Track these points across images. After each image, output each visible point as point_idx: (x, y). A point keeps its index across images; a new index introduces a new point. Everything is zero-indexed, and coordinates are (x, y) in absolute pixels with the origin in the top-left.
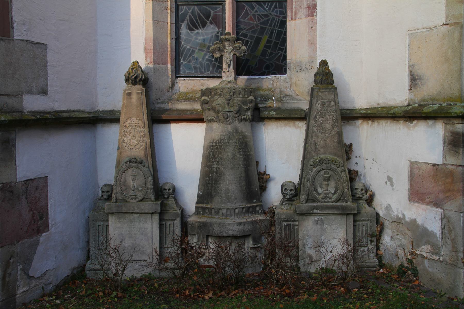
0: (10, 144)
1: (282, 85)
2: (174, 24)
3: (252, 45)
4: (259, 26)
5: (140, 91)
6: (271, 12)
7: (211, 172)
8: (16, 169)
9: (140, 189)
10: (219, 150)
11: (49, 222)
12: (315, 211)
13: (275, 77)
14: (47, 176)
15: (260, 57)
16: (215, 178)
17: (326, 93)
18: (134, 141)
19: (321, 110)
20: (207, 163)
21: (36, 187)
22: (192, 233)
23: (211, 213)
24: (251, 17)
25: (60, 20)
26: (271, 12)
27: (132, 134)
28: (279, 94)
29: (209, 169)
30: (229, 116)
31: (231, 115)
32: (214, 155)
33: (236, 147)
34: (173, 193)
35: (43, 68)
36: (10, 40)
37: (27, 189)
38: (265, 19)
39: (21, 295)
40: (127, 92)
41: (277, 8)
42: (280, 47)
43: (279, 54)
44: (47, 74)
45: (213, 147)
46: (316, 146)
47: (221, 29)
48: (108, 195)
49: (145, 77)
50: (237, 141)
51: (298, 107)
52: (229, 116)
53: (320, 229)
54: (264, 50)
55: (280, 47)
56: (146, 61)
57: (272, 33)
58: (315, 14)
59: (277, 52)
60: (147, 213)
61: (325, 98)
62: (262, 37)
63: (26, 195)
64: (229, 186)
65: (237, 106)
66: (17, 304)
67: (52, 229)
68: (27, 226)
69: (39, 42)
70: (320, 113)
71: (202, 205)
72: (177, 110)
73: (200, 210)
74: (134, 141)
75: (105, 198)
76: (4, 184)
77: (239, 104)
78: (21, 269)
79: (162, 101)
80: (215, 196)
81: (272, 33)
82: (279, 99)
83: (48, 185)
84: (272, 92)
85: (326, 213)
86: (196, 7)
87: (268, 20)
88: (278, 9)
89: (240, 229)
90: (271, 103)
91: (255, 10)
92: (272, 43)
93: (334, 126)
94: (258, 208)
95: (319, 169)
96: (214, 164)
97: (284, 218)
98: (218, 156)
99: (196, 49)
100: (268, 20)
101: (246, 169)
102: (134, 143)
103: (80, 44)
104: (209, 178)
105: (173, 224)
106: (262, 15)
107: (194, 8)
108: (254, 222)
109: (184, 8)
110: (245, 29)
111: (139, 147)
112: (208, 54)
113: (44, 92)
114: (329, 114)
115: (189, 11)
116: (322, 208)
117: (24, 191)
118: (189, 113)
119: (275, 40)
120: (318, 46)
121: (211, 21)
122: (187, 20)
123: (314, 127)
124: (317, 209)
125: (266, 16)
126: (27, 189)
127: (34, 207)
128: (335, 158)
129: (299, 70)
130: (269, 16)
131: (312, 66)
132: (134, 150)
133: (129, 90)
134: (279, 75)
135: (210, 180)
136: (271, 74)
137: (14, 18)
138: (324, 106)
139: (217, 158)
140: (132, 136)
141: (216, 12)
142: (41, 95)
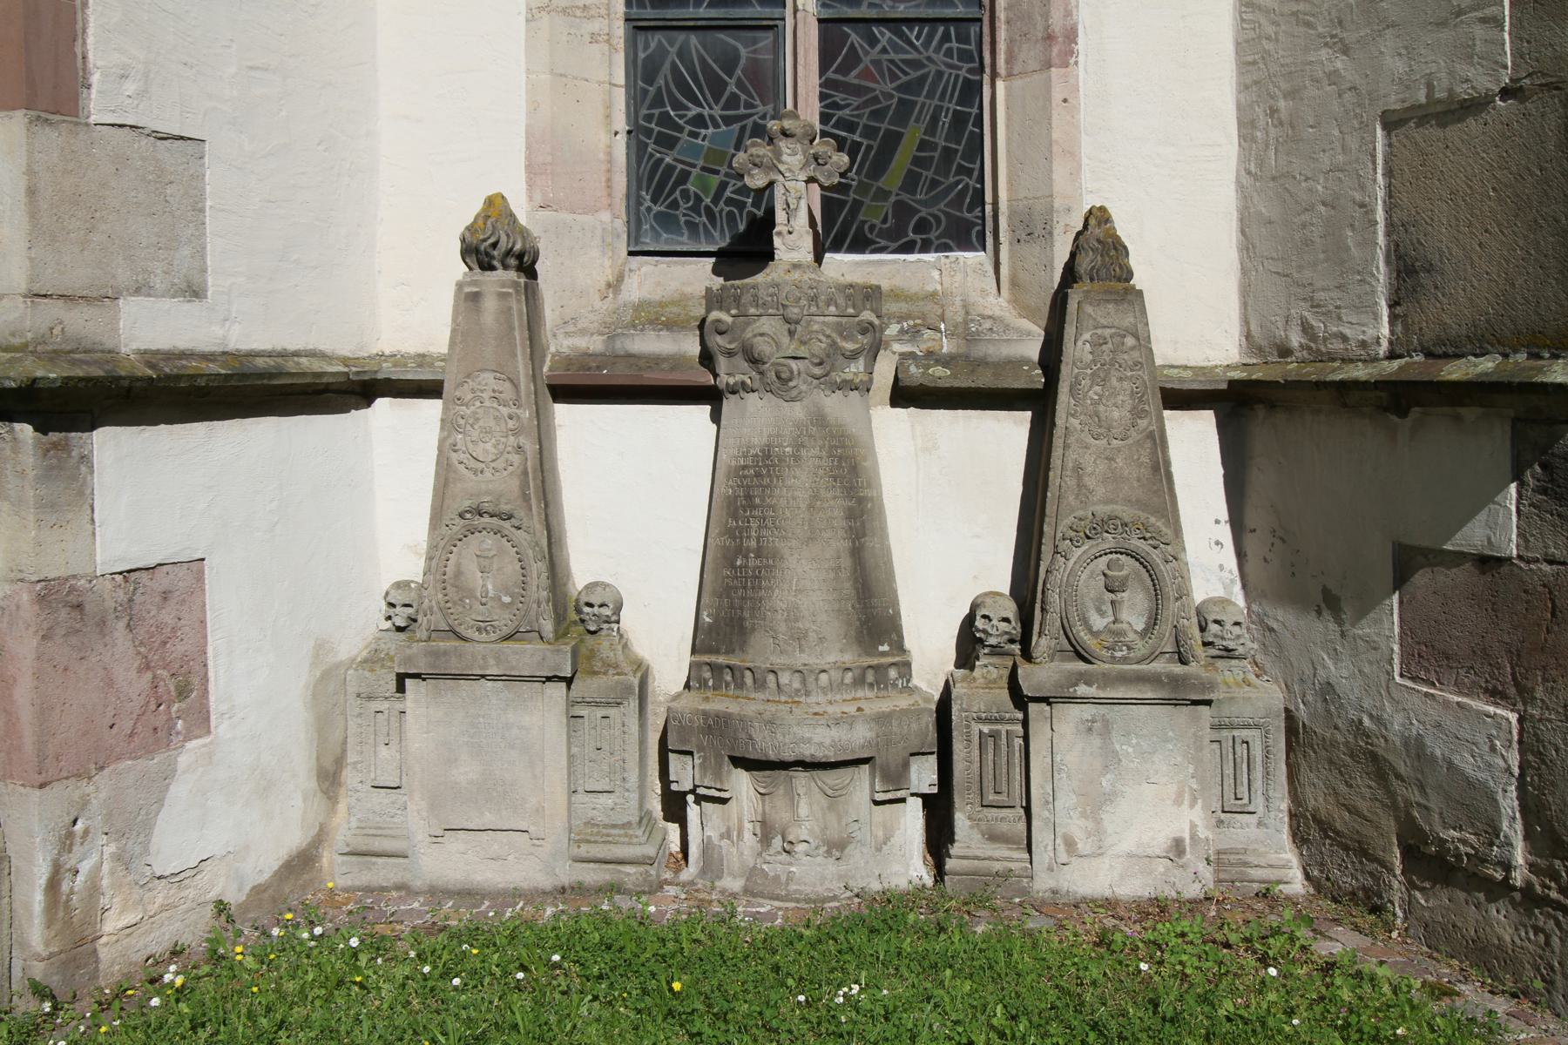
0: (74, 454)
3: (871, 157)
5: (509, 287)
6: (931, 53)
7: (741, 549)
8: (94, 534)
9: (507, 599)
10: (766, 481)
12: (1082, 690)
13: (947, 257)
15: (897, 195)
16: (754, 571)
18: (489, 446)
19: (1094, 362)
21: (164, 593)
23: (740, 685)
25: (251, 68)
26: (931, 53)
27: (481, 423)
31: (802, 369)
32: (749, 497)
35: (189, 214)
36: (77, 124)
37: (131, 600)
38: (914, 74)
39: (115, 938)
40: (468, 289)
41: (951, 42)
42: (963, 163)
43: (960, 187)
44: (205, 234)
46: (1079, 478)
48: (406, 616)
51: (1022, 357)
52: (796, 373)
53: (1100, 748)
54: (910, 171)
55: (963, 163)
56: (531, 199)
57: (935, 119)
58: (1072, 61)
59: (952, 180)
60: (531, 679)
61: (1105, 323)
62: (902, 130)
63: (128, 618)
64: (800, 596)
65: (820, 341)
66: (101, 967)
67: (221, 727)
68: (135, 716)
69: (176, 133)
70: (1089, 371)
71: (713, 658)
72: (630, 356)
73: (707, 675)
75: (397, 624)
76: (49, 581)
77: (828, 337)
78: (112, 855)
79: (580, 326)
80: (753, 629)
81: (935, 119)
82: (960, 330)
83: (207, 587)
84: (936, 307)
85: (1120, 695)
87: (923, 78)
88: (955, 45)
90: (934, 340)
91: (879, 47)
92: (935, 149)
93: (1137, 413)
94: (893, 673)
95: (1094, 551)
98: (763, 500)
100: (923, 78)
101: (853, 542)
102: (487, 452)
103: (319, 144)
104: (736, 572)
106: (902, 61)
109: (656, 40)
110: (848, 105)
112: (733, 182)
113: (194, 291)
114: (1120, 374)
115: (670, 49)
116: (1107, 680)
117: (121, 605)
119: (946, 140)
120: (1085, 161)
121: (739, 79)
122: (665, 76)
123: (1073, 415)
124: (1089, 684)
126: (131, 600)
127: (156, 657)
130: (924, 66)
132: (488, 474)
134: (962, 253)
135: (737, 577)
137: (91, 56)
139: (758, 506)
140: (482, 432)
141: (755, 52)
142: (181, 299)
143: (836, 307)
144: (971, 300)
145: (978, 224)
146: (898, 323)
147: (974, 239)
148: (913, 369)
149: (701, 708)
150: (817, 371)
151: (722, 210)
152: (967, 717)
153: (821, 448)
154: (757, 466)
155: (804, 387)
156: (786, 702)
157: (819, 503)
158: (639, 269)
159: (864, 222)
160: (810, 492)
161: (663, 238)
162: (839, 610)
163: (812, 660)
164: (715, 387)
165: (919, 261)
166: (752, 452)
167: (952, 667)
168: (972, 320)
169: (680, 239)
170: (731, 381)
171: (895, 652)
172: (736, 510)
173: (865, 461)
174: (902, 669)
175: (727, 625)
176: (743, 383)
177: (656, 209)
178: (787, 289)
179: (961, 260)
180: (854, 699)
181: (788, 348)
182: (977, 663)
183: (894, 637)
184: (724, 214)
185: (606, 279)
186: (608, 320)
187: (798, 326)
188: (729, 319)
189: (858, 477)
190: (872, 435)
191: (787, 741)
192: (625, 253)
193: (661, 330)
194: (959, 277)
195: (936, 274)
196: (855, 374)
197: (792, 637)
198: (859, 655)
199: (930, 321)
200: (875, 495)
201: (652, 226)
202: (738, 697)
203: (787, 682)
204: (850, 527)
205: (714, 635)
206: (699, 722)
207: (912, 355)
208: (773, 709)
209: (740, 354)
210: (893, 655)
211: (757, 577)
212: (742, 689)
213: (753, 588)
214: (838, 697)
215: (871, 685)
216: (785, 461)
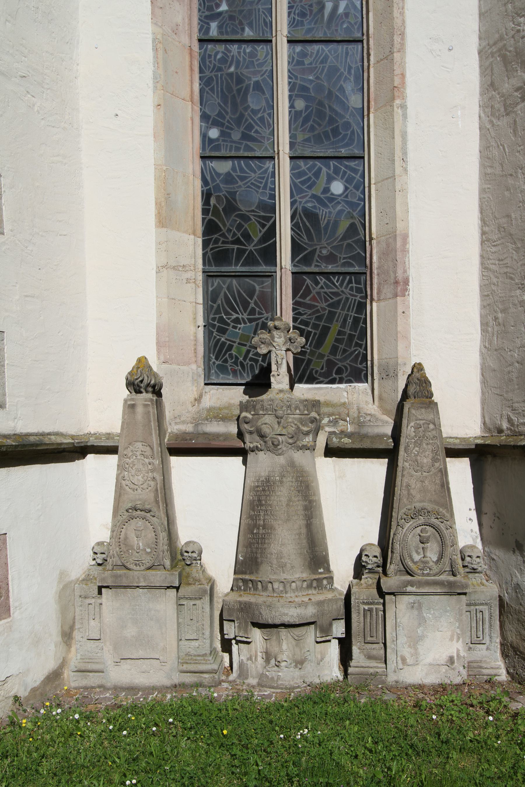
1: (360, 399)
2: (201, 304)
4: (326, 309)
6: (343, 289)
9: (148, 550)
10: (268, 493)
11: (11, 602)
12: (409, 589)
13: (350, 386)
14: (6, 534)
15: (328, 356)
16: (262, 535)
17: (423, 410)
18: (140, 478)
19: (415, 436)
23: (256, 589)
24: (314, 296)
25: (26, 296)
27: (136, 466)
28: (357, 412)
31: (284, 440)
32: (259, 500)
33: (292, 488)
34: (198, 558)
38: (336, 299)
40: (129, 403)
43: (356, 352)
45: (258, 489)
46: (409, 490)
47: (270, 313)
49: (155, 381)
54: (334, 345)
56: (159, 358)
57: (345, 320)
58: (407, 294)
59: (353, 349)
60: (160, 587)
65: (292, 427)
72: (205, 433)
73: (241, 584)
74: (140, 478)
77: (296, 425)
79: (182, 419)
80: (262, 563)
81: (345, 320)
82: (356, 421)
86: (234, 281)
88: (354, 285)
91: (320, 286)
92: (345, 335)
93: (435, 460)
94: (325, 582)
95: (415, 524)
96: (259, 515)
98: (266, 502)
99: (235, 342)
100: (339, 302)
101: (307, 521)
102: (138, 480)
106: (330, 292)
107: (231, 282)
108: (320, 603)
109: (217, 282)
110: (306, 313)
111: (146, 487)
115: (224, 286)
116: (420, 584)
118: (221, 438)
122: (221, 299)
123: (406, 461)
125: (336, 294)
128: (437, 507)
129: (385, 377)
130: (340, 295)
131: (404, 371)
133: (132, 399)
135: (254, 538)
138: (420, 429)
141: (263, 288)
144: (361, 406)
145: (364, 370)
146: (328, 417)
147: (363, 377)
148: (334, 439)
150: (291, 441)
151: (247, 364)
154: (263, 486)
155: (284, 449)
156: (277, 597)
159: (313, 369)
160: (287, 498)
165: (338, 388)
166: (261, 479)
167: (351, 578)
168: (362, 416)
169: (228, 377)
170: (252, 446)
174: (330, 580)
176: (257, 447)
178: (277, 402)
179: (357, 387)
180: (307, 595)
181: (277, 430)
182: (363, 577)
183: (326, 565)
184: (249, 365)
187: (282, 420)
194: (356, 396)
195: (345, 394)
196: (308, 442)
197: (279, 566)
198: (310, 574)
200: (317, 499)
201: (215, 371)
202: (255, 594)
204: (306, 514)
206: (237, 606)
207: (334, 433)
209: (256, 433)
210: (325, 574)
213: (262, 543)
214: (300, 594)
215: (315, 588)
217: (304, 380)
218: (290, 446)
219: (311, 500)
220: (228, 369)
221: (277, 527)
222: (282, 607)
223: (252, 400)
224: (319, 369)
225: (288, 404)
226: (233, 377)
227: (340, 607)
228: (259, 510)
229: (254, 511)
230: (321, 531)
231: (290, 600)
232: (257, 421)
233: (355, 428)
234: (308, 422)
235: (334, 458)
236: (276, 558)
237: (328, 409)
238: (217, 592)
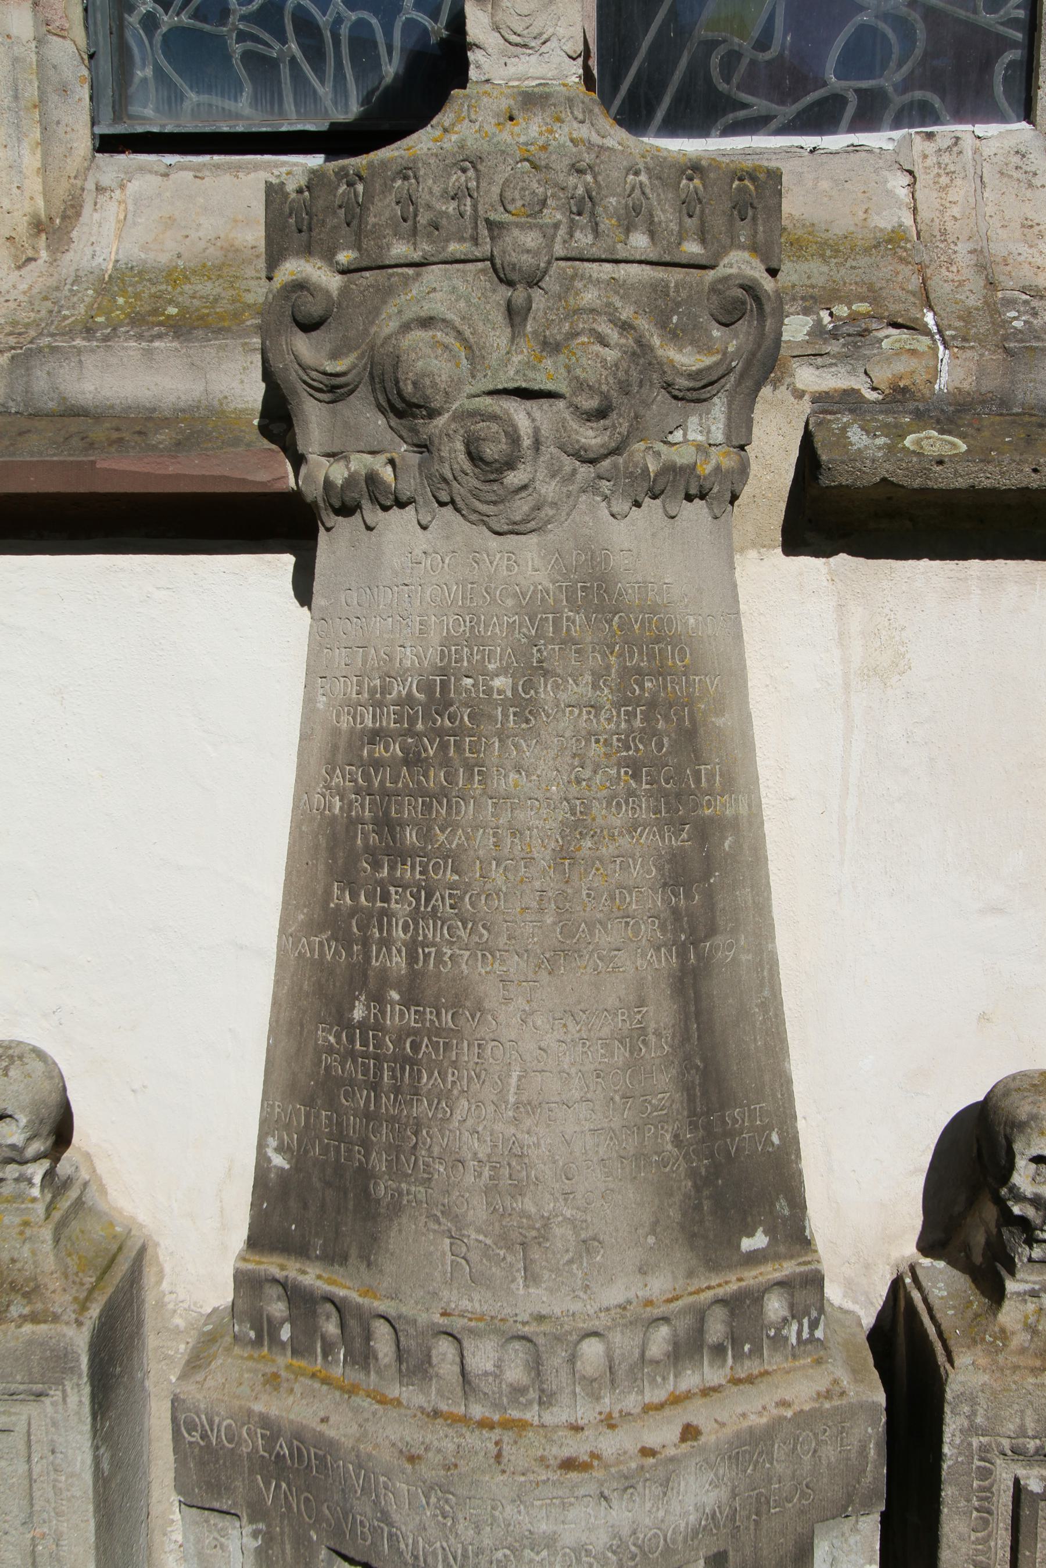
10: (436, 778)
13: (930, 136)
16: (398, 1042)
20: (328, 893)
22: (216, 1505)
28: (978, 283)
29: (350, 954)
30: (527, 442)
31: (546, 430)
32: (386, 824)
33: (596, 750)
45: (379, 751)
50: (606, 695)
52: (527, 442)
65: (603, 341)
72: (75, 412)
73: (278, 1308)
77: (625, 327)
80: (396, 1208)
82: (982, 326)
84: (906, 270)
89: (625, 1532)
90: (913, 352)
94: (775, 1306)
96: (384, 913)
97: (1022, 1432)
98: (426, 835)
101: (683, 955)
104: (351, 1040)
105: (21, 1428)
118: (163, 437)
134: (969, 127)
135: (352, 1054)
136: (888, 116)
143: (652, 234)
144: (998, 249)
145: (1013, 44)
146: (806, 311)
147: (999, 89)
148: (857, 437)
149: (258, 1407)
150: (591, 437)
151: (338, 21)
152: (984, 1449)
153: (597, 676)
154: (410, 732)
155: (549, 489)
156: (485, 1424)
157: (588, 843)
158: (122, 187)
159: (711, 45)
160: (562, 813)
161: (187, 105)
162: (637, 1157)
163: (558, 1305)
164: (295, 498)
165: (855, 148)
166: (398, 690)
167: (909, 1249)
168: (1010, 303)
169: (229, 105)
170: (339, 473)
171: (782, 1249)
172: (352, 859)
173: (720, 712)
174: (803, 1296)
175: (328, 1184)
176: (372, 479)
177: (167, 20)
178: (504, 172)
179: (968, 143)
180: (676, 1400)
181: (505, 362)
182: (1011, 1286)
183: (782, 1207)
184: (344, 31)
185: (28, 209)
186: (25, 316)
187: (537, 294)
188: (331, 281)
189: (699, 759)
190: (738, 637)
191: (487, 1542)
192: (83, 143)
193: (160, 336)
194: (961, 191)
195: (899, 183)
196: (699, 447)
197: (504, 1240)
198: (690, 1274)
199: (893, 307)
200: (743, 810)
201: (158, 71)
202: (352, 1390)
203: (489, 1367)
204: (675, 911)
205: (293, 1204)
206: (252, 1442)
207: (849, 400)
208: (450, 1447)
209: (364, 390)
210: (777, 1257)
211: (406, 1060)
212: (366, 1367)
213: (397, 1090)
214: (632, 1402)
215: (719, 1350)
216: (492, 718)
217: (660, 115)
218: (585, 471)
219: (711, 819)
220: (227, 57)
221: (491, 993)
222: (518, 1499)
223: (342, 174)
224: (744, 44)
225: (578, 184)
226: (255, 101)
227: (863, 1451)
228: (381, 883)
229: (351, 885)
230: (764, 1006)
231: (575, 1447)
232: (376, 311)
233: (982, 372)
234: (704, 318)
235: (842, 560)
236: (487, 1191)
237: (803, 267)
238: (160, 1304)
